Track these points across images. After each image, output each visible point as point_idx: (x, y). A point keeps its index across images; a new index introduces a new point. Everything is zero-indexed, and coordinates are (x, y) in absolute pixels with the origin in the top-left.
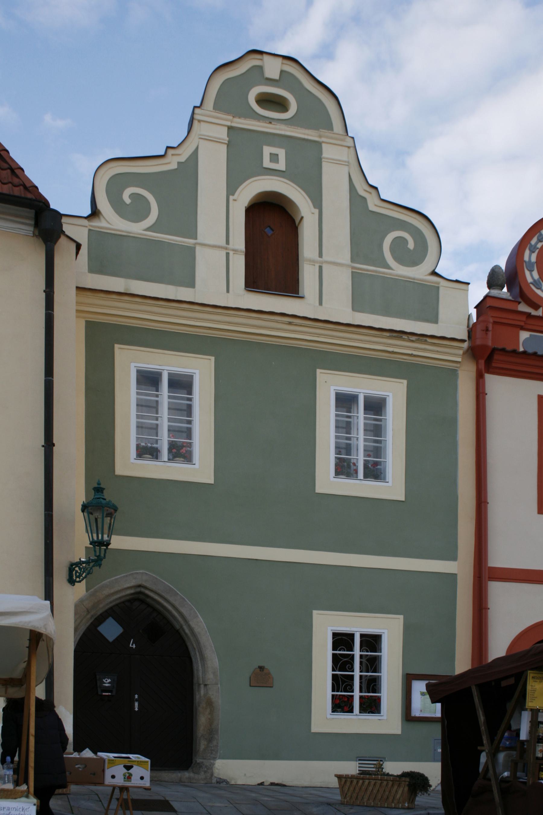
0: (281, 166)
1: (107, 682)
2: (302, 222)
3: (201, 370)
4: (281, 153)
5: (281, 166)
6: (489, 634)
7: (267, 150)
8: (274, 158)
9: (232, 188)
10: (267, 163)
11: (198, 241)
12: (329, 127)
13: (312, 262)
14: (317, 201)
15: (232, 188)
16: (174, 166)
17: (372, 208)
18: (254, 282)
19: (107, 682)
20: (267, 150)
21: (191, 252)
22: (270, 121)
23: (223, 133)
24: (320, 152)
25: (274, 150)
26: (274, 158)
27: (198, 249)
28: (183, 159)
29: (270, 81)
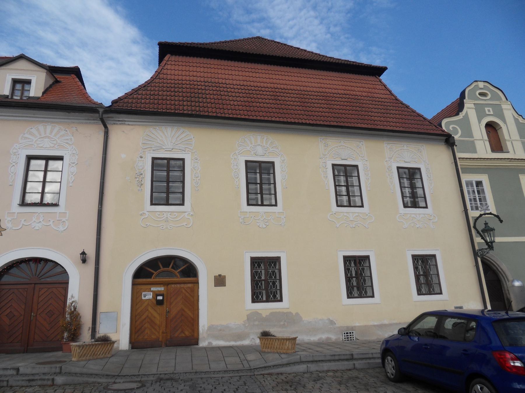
0: (492, 113)
1: (123, 156)
2: (48, 85)
3: (484, 179)
4: (491, 109)
5: (492, 113)
6: (49, 112)
7: (486, 109)
8: (489, 111)
9: (480, 122)
10: (487, 113)
11: (475, 138)
12: (500, 99)
13: (509, 141)
14: (505, 122)
15: (480, 122)
16: (462, 117)
17: (521, 122)
18: (493, 150)
19: (123, 156)
20: (486, 109)
21: (473, 143)
22: (485, 100)
23: (473, 106)
24: (501, 107)
25: (488, 109)
26: (489, 111)
27: (475, 141)
28: (464, 115)
29: (481, 89)
